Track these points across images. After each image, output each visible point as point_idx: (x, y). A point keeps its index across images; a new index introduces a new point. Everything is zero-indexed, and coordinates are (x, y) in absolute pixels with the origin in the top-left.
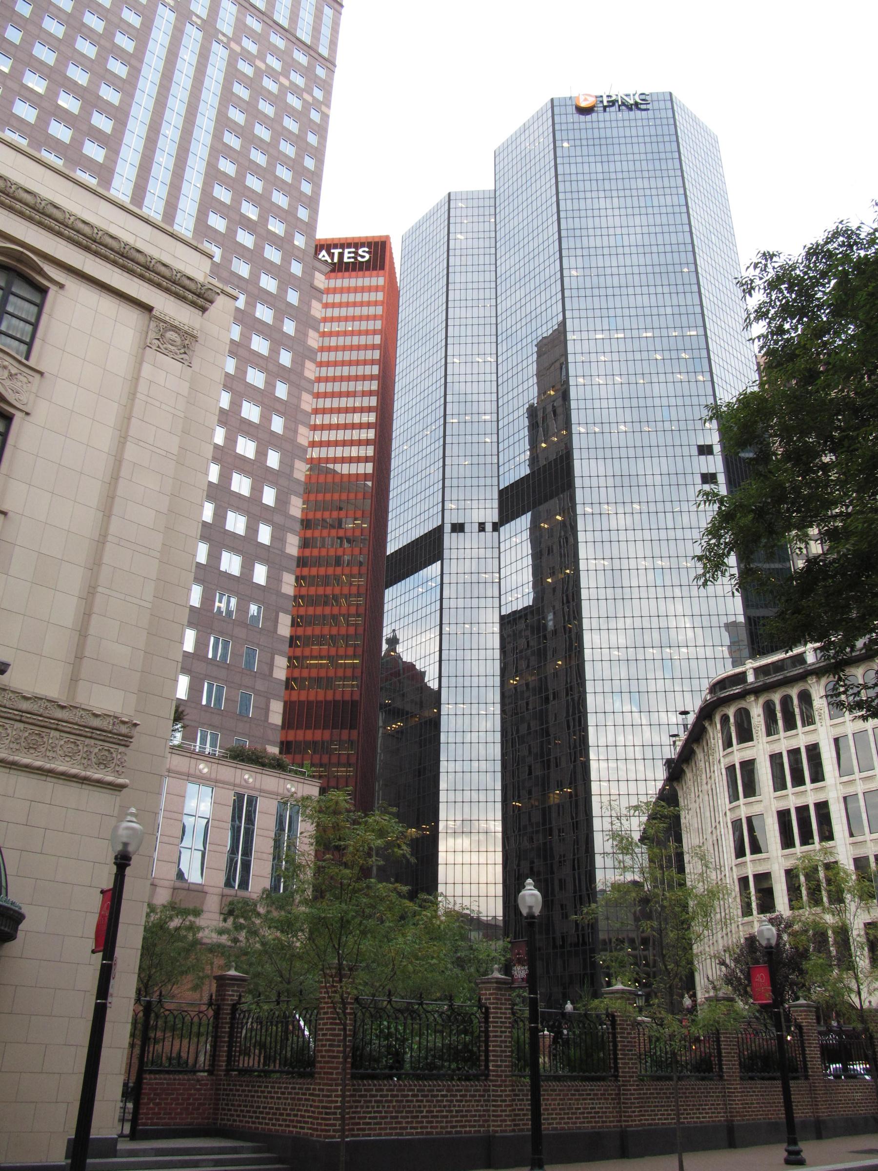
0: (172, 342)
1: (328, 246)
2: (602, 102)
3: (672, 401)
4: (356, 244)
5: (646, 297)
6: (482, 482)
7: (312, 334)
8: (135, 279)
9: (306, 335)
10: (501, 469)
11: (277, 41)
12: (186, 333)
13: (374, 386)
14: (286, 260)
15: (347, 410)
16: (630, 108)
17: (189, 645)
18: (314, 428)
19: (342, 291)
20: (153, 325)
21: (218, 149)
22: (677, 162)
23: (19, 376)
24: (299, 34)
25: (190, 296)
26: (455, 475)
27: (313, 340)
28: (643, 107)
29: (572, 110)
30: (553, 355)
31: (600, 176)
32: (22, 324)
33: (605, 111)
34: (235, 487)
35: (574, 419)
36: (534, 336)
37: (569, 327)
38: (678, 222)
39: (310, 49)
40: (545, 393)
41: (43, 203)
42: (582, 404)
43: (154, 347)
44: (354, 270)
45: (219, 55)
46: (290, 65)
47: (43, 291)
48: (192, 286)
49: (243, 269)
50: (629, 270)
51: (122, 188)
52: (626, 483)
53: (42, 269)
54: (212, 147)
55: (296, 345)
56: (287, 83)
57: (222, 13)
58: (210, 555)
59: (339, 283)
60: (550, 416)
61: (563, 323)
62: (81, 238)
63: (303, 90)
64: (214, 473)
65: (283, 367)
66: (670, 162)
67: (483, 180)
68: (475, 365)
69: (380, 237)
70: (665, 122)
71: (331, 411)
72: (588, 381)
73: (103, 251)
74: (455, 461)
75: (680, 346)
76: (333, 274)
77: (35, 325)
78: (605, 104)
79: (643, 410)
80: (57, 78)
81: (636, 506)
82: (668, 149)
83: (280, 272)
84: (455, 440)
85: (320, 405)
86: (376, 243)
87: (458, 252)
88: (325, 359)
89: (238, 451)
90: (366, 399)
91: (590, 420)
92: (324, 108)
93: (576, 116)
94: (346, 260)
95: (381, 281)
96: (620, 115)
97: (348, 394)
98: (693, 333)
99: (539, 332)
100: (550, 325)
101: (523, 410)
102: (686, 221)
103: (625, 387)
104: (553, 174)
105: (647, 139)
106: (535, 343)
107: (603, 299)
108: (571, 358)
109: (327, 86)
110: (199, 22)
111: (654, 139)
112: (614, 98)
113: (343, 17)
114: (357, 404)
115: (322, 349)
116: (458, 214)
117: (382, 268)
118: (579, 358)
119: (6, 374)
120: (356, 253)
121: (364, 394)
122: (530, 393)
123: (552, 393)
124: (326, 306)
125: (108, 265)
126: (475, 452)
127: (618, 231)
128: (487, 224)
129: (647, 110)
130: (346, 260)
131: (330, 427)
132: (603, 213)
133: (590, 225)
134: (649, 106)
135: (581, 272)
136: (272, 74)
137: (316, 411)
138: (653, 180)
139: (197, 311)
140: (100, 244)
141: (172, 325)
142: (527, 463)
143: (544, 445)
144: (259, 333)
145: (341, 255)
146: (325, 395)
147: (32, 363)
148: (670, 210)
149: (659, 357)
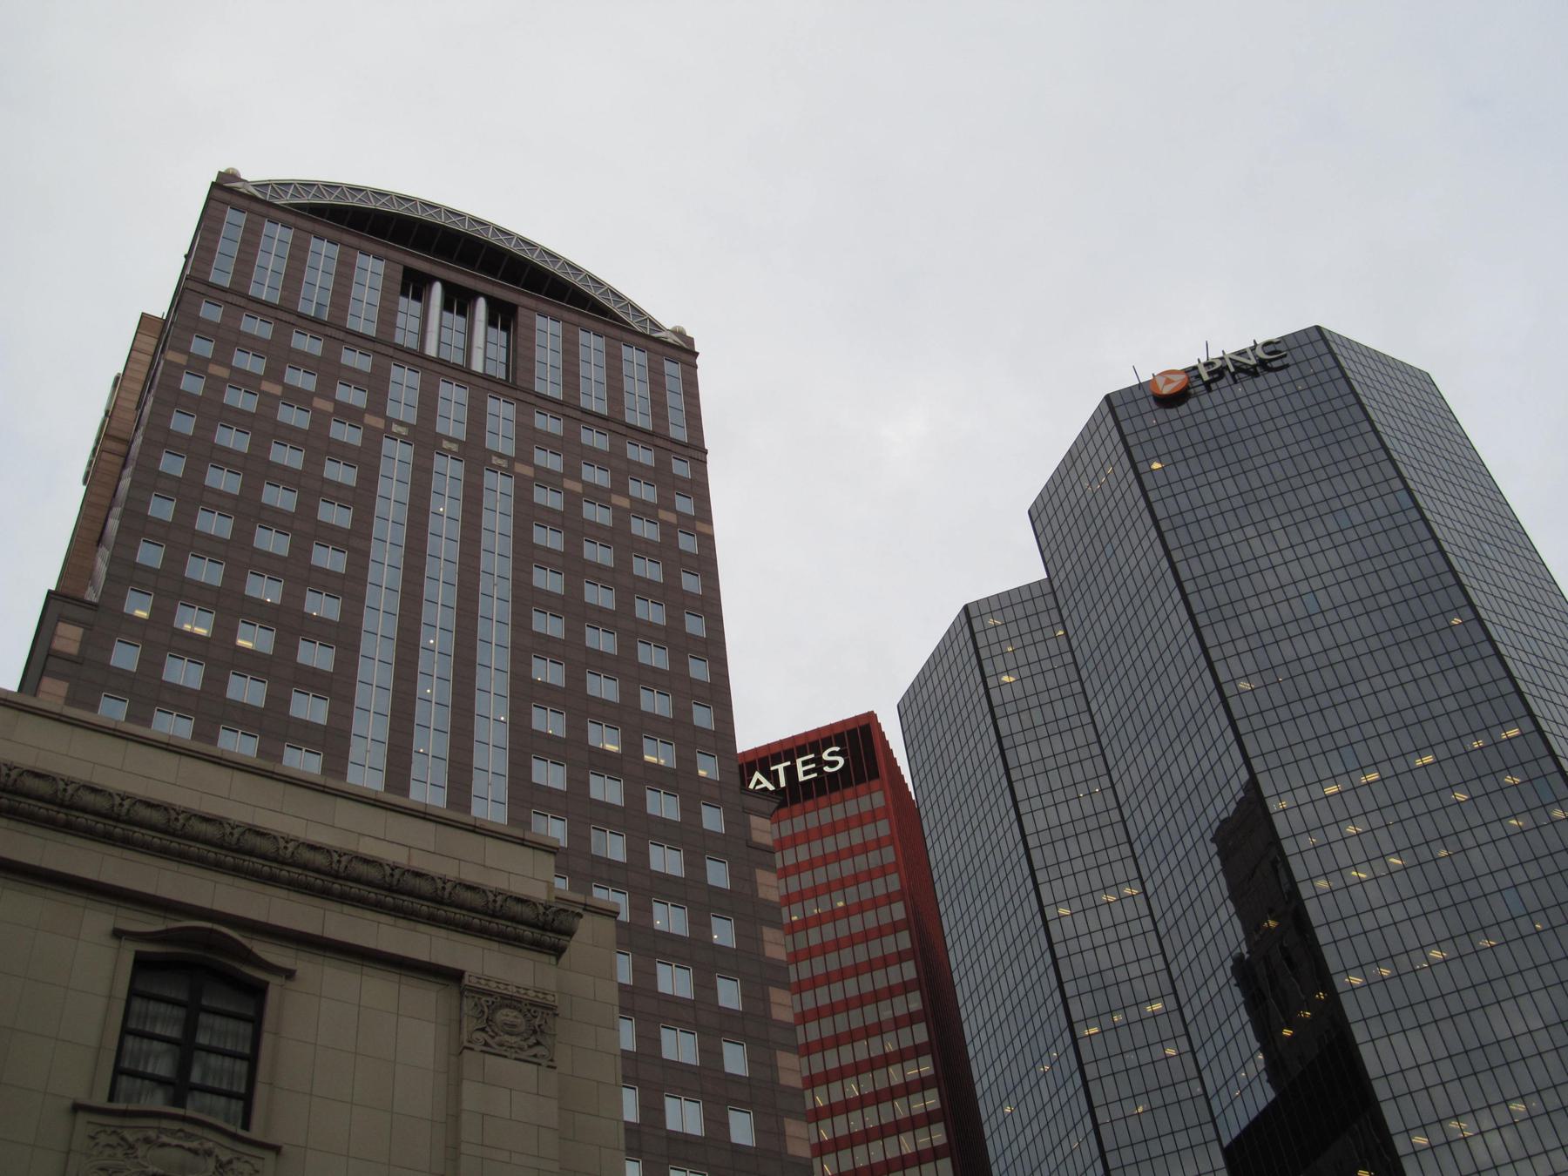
0: (510, 1029)
1: (763, 759)
2: (1199, 376)
3: (1519, 875)
4: (812, 743)
5: (1397, 692)
6: (1183, 1141)
7: (769, 934)
8: (422, 927)
9: (760, 940)
10: (1215, 1103)
11: (595, 440)
12: (533, 1004)
13: (915, 1002)
14: (694, 864)
15: (872, 1065)
16: (1252, 372)
17: (631, 1113)
18: (816, 1115)
19: (808, 837)
20: (468, 1004)
21: (526, 645)
22: (1371, 437)
23: (236, 1165)
24: (629, 418)
25: (528, 933)
26: (1123, 1140)
27: (775, 946)
28: (1275, 364)
29: (1145, 406)
30: (1251, 850)
31: (1237, 502)
32: (228, 1062)
33: (1209, 390)
34: (668, 1052)
35: (1333, 963)
36: (1203, 822)
37: (1267, 790)
38: (1411, 539)
39: (653, 437)
40: (1258, 927)
41: (237, 832)
42: (1339, 931)
43: (478, 1047)
44: (821, 792)
45: (499, 490)
46: (624, 471)
47: (258, 992)
48: (527, 912)
49: (614, 847)
50: (1348, 652)
51: (366, 772)
52: (1477, 1057)
53: (250, 952)
54: (515, 646)
55: (745, 962)
56: (625, 503)
57: (490, 423)
58: (644, 1107)
59: (799, 824)
60: (1283, 968)
61: (1253, 785)
62: (311, 878)
63: (657, 507)
64: (627, 1035)
65: (729, 1013)
66: (1358, 441)
67: (1022, 565)
68: (1104, 911)
69: (856, 718)
70: (1324, 377)
71: (842, 1073)
72: (1337, 882)
73: (355, 889)
74: (1116, 1112)
75: (1497, 764)
76: (784, 811)
77: (252, 1060)
78: (1206, 377)
79: (1465, 909)
80: (230, 606)
81: (1518, 1107)
82: (1378, 478)
83: (684, 835)
84: (1105, 1068)
85: (809, 1003)
86: (852, 733)
87: (1011, 708)
88: (805, 974)
89: (670, 1126)
90: (905, 1033)
91: (1366, 956)
92: (700, 527)
93: (1160, 413)
94: (801, 778)
95: (878, 799)
96: (1239, 389)
97: (867, 1032)
98: (1513, 732)
99: (1211, 813)
100: (1227, 795)
101: (1225, 974)
102: (1424, 534)
103: (1416, 874)
104: (1148, 521)
105: (1304, 415)
106: (1208, 836)
107: (1316, 717)
108: (1288, 847)
109: (698, 489)
110: (454, 447)
111: (1315, 411)
112: (1218, 364)
113: (701, 374)
114: (890, 1047)
115: (788, 900)
116: (993, 638)
117: (874, 774)
118: (1308, 841)
119: (212, 1163)
120: (819, 761)
121: (898, 1023)
122: (1225, 933)
123: (1272, 924)
124: (784, 873)
125: (369, 915)
126: (1152, 1083)
127: (1304, 587)
128: (1052, 644)
129: (1286, 366)
130: (801, 778)
131: (847, 1106)
132: (1264, 563)
133: (1248, 592)
134: (1286, 361)
135: (1257, 681)
136: (595, 494)
137: (811, 1082)
138: (1337, 481)
139: (545, 958)
140: (347, 878)
141: (503, 997)
142: (1264, 1077)
143: (1287, 1032)
144: (668, 958)
145: (791, 772)
146: (822, 1045)
147: (255, 1133)
148: (1388, 523)
149: (1461, 797)
